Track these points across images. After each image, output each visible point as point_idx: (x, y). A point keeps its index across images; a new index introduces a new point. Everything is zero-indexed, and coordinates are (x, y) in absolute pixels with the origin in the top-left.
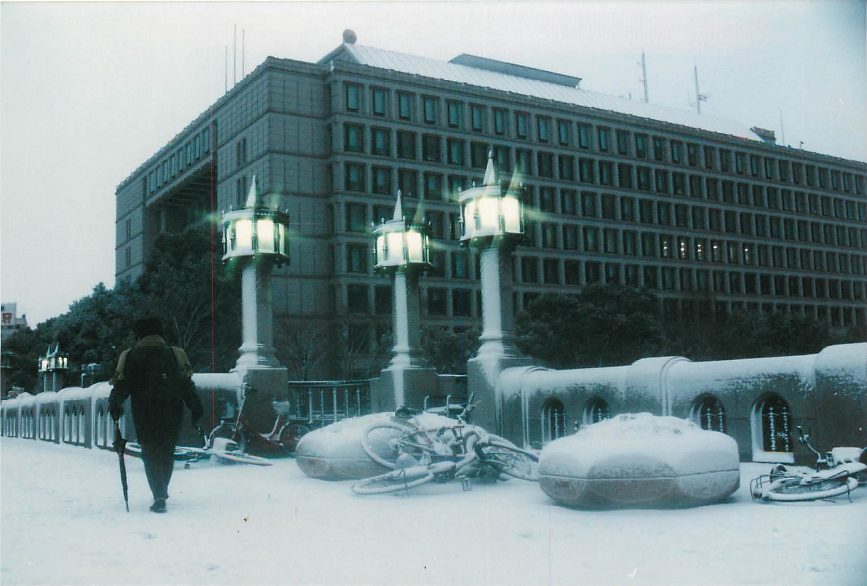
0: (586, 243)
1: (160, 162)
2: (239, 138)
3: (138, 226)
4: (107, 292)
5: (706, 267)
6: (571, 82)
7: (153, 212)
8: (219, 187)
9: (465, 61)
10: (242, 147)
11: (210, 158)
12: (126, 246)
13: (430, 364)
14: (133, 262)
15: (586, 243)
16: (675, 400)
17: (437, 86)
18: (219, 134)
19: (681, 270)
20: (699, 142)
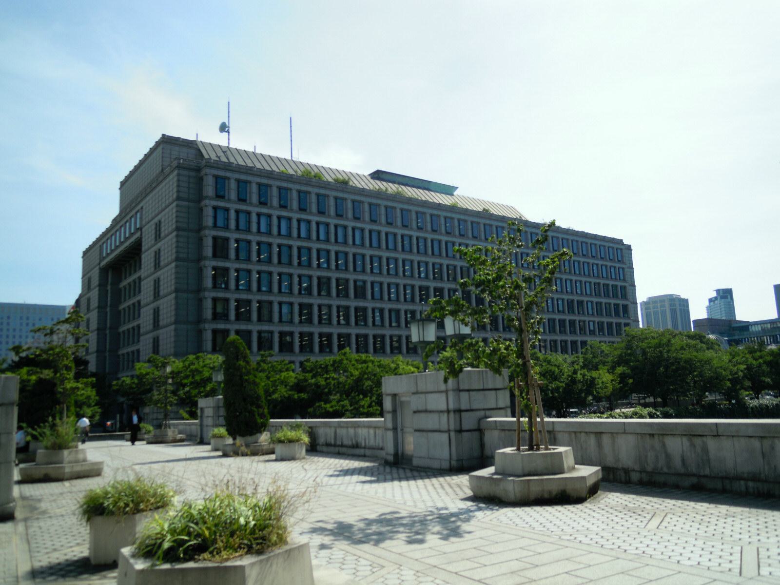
0: (405, 295)
1: (104, 239)
2: (156, 220)
3: (95, 281)
4: (745, 327)
5: (398, 306)
6: (448, 190)
7: (104, 271)
8: (143, 256)
9: (378, 175)
10: (158, 226)
11: (138, 235)
12: (87, 296)
13: (122, 385)
14: (91, 308)
15: (405, 295)
16: (17, 444)
17: (242, 170)
18: (144, 217)
19: (390, 311)
20: (228, 174)
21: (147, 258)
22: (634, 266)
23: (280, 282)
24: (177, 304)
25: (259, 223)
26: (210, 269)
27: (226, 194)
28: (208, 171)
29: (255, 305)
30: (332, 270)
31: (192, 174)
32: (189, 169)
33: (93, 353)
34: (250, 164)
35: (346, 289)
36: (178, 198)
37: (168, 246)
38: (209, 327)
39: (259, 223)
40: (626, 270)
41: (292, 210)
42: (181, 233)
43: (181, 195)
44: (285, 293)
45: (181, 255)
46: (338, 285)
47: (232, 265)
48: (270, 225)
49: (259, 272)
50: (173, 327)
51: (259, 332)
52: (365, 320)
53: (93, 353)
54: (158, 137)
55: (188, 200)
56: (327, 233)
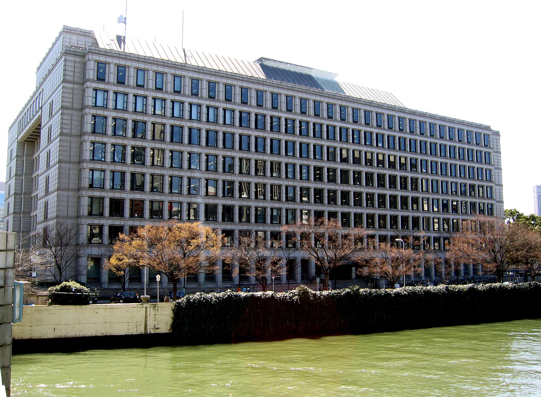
2: (50, 101)
21: (44, 133)
22: (502, 150)
23: (207, 161)
24: (60, 173)
25: (225, 117)
26: (89, 143)
27: (107, 78)
28: (90, 56)
29: (167, 180)
30: (235, 150)
31: (78, 59)
32: (75, 54)
33: (52, 219)
34: (201, 65)
35: (321, 175)
36: (64, 81)
37: (55, 123)
38: (87, 194)
39: (225, 117)
40: (492, 154)
41: (219, 101)
42: (66, 111)
43: (67, 78)
44: (157, 166)
45: (65, 131)
46: (328, 172)
47: (148, 145)
48: (200, 113)
49: (171, 152)
50: (56, 193)
51: (152, 202)
52: (407, 206)
53: (52, 219)
54: (61, 29)
55: (73, 83)
56: (200, 113)
